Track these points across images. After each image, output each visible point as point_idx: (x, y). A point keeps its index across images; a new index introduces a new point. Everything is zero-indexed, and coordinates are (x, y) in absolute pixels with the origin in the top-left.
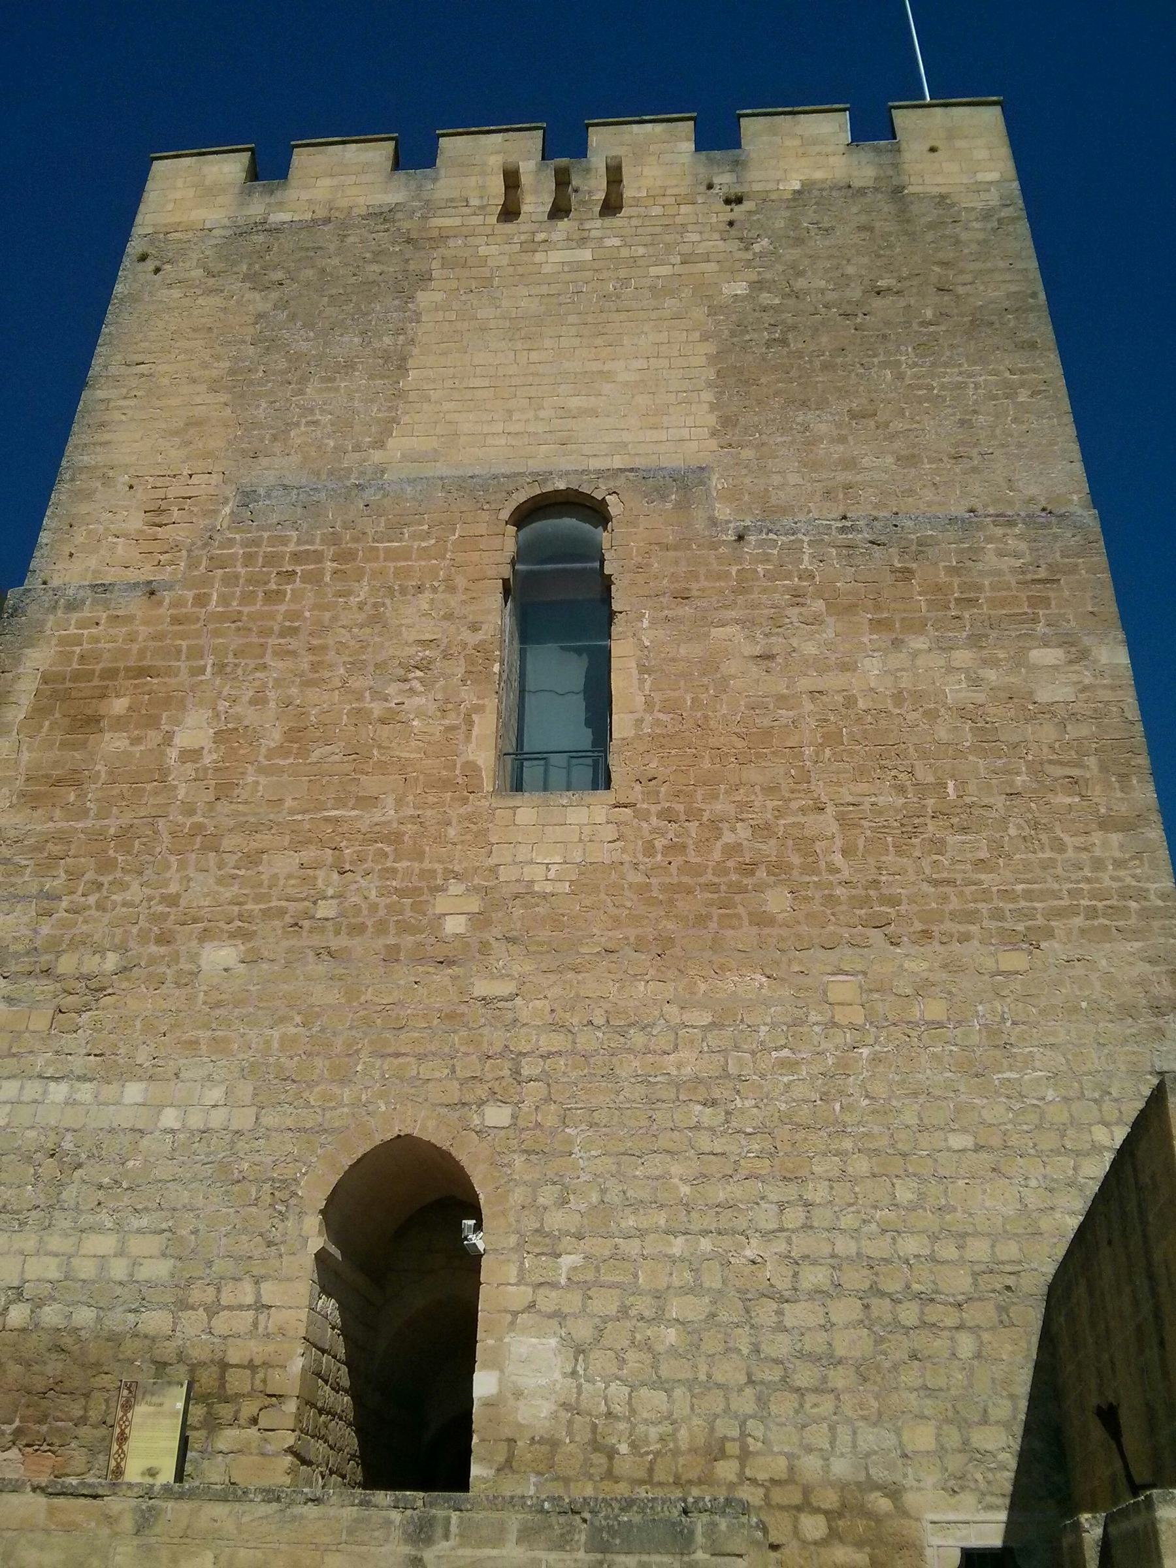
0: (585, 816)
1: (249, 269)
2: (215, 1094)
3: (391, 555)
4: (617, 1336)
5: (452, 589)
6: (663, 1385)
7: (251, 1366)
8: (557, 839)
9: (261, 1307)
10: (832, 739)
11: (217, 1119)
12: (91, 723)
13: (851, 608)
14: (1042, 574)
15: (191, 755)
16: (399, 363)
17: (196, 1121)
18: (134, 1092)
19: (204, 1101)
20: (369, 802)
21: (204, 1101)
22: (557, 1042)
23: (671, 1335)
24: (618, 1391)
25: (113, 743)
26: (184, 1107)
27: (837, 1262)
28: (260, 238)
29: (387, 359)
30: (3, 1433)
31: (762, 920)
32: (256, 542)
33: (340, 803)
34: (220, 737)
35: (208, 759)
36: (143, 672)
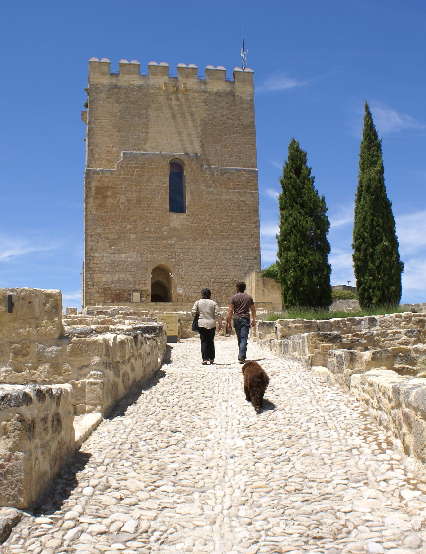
0: (182, 216)
1: (377, 335)
2: (135, 256)
3: (150, 168)
4: (189, 287)
5: (160, 176)
6: (195, 293)
7: (145, 291)
8: (178, 220)
9: (145, 284)
10: (218, 207)
11: (136, 259)
12: (106, 197)
13: (222, 184)
14: (249, 181)
15: (123, 203)
16: (146, 126)
17: (133, 260)
18: (124, 255)
19: (133, 257)
20: (151, 213)
21: (133, 257)
22: (181, 250)
23: (196, 287)
24: (190, 293)
25: (110, 200)
26: (131, 258)
27: (215, 279)
28: (116, 90)
29: (145, 124)
30: (423, 363)
31: (208, 234)
32: (127, 164)
33: (147, 213)
34: (127, 200)
35: (126, 204)
36: (112, 188)
